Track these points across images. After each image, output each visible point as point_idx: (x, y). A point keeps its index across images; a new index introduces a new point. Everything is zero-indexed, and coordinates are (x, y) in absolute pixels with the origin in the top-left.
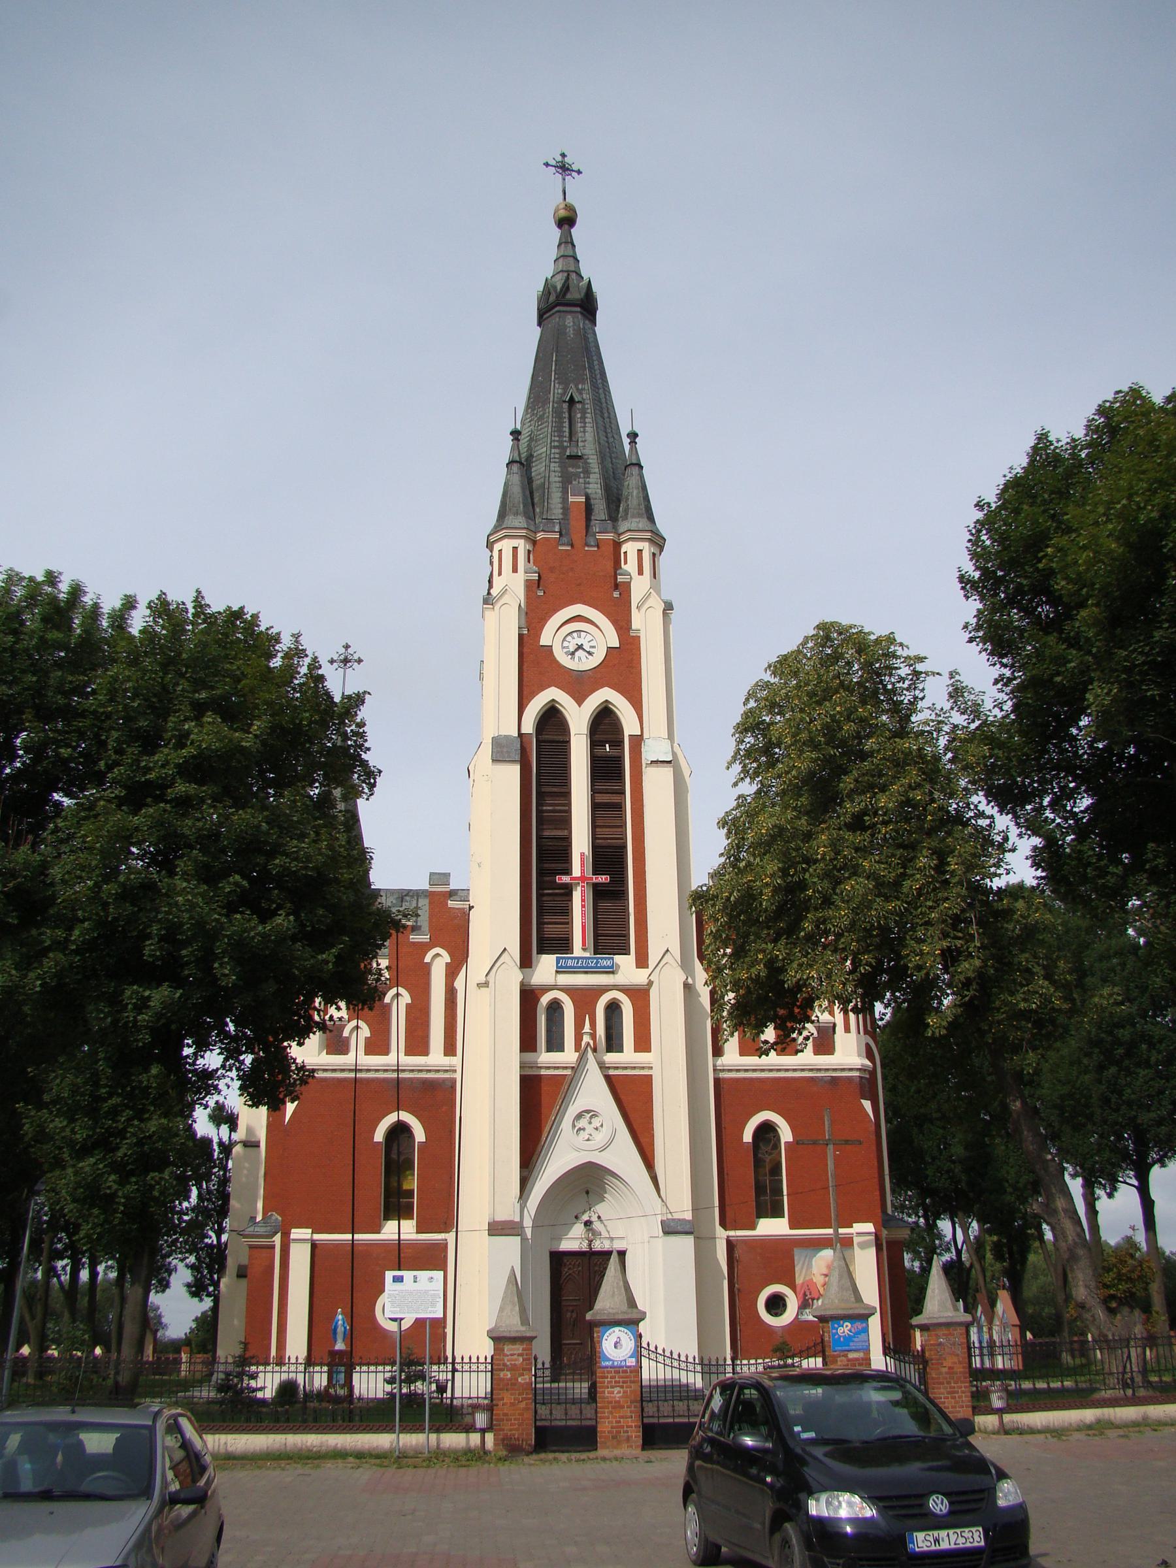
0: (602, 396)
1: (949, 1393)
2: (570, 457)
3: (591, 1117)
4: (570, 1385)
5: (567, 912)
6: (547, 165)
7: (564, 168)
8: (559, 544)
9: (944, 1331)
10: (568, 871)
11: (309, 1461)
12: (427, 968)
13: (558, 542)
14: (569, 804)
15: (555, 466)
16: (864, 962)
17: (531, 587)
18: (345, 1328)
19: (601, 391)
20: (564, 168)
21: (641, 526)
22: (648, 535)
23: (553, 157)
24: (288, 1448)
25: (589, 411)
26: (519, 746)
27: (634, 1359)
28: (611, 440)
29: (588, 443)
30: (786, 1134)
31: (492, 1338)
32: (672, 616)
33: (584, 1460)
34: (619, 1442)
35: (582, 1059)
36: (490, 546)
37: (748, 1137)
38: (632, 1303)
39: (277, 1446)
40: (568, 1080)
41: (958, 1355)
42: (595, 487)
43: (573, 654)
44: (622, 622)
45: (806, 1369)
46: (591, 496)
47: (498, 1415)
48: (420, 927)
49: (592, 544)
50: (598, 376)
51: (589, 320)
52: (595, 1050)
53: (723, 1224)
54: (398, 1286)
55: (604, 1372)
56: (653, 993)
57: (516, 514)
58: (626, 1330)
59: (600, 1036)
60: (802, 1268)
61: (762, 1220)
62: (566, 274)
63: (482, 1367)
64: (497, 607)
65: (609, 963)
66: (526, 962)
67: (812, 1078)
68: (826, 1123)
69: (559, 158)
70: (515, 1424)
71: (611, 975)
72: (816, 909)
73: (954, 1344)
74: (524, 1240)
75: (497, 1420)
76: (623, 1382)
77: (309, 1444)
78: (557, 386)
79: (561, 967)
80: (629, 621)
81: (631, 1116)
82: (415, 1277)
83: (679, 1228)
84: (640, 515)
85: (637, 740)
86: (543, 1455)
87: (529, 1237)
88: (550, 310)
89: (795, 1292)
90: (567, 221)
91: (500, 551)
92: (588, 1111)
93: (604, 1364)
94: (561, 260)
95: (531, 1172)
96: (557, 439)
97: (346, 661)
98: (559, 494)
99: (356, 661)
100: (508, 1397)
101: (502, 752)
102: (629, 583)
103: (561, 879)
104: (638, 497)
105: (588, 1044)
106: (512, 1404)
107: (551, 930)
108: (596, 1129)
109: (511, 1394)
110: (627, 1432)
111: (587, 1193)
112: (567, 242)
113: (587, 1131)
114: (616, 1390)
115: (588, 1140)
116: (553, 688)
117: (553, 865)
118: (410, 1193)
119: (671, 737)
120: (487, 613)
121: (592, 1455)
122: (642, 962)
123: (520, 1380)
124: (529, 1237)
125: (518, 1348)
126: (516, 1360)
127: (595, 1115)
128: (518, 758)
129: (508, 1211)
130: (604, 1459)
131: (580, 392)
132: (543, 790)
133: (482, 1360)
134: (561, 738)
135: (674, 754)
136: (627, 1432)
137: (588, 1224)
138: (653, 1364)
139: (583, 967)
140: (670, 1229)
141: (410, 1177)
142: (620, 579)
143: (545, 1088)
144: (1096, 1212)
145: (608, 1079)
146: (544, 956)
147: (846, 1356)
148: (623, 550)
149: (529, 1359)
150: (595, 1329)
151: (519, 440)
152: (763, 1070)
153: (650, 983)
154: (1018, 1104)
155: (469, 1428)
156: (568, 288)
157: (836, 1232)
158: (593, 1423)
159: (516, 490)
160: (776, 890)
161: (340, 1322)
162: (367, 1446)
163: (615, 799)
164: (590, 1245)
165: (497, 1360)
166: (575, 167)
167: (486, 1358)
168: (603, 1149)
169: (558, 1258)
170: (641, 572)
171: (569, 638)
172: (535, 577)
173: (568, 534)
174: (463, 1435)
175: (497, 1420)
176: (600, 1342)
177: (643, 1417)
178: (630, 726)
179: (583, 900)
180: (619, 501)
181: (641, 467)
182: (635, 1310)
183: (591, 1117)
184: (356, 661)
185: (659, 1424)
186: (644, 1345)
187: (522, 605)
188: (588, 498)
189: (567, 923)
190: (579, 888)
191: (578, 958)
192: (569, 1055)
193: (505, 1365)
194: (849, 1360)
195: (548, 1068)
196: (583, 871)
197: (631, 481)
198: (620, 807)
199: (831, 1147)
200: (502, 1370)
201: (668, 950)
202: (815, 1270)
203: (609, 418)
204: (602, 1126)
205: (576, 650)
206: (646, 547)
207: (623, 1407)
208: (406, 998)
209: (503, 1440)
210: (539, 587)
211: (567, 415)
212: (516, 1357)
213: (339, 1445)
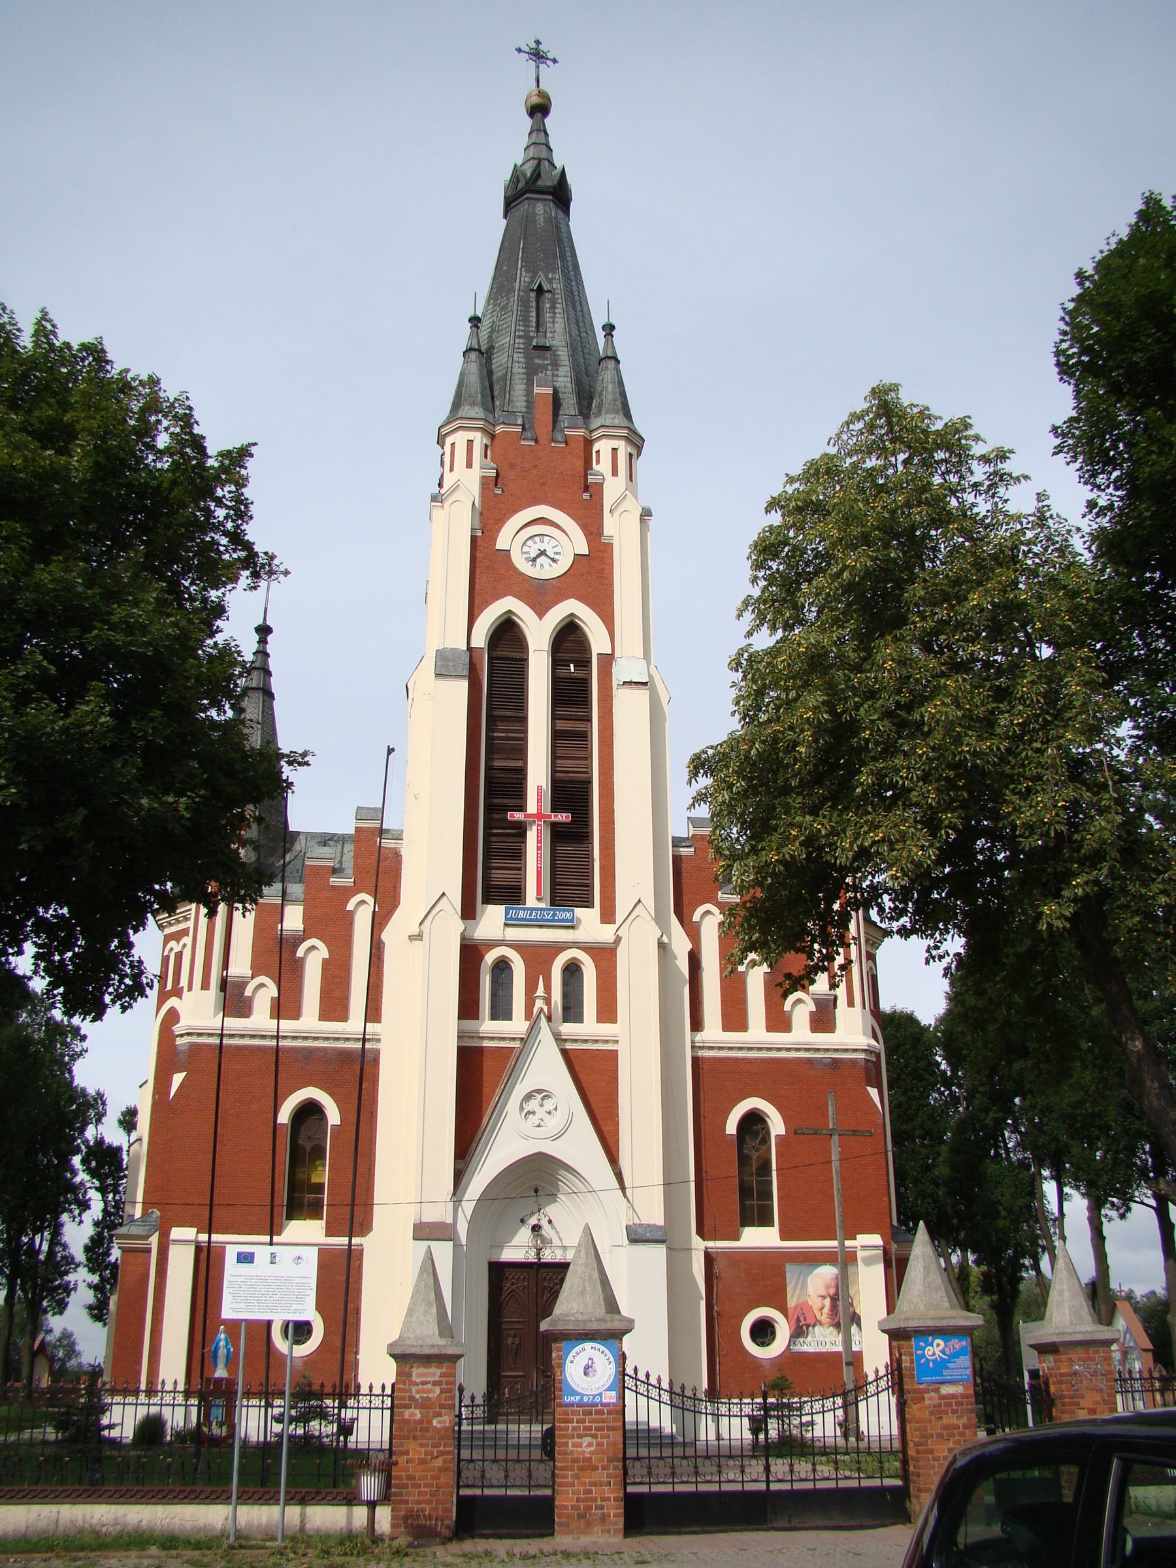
0: (575, 288)
2: (536, 348)
3: (543, 1099)
4: (513, 1427)
5: (518, 855)
6: (519, 50)
7: (538, 55)
8: (521, 439)
9: (1079, 1353)
10: (522, 808)
11: (81, 1554)
12: (350, 916)
13: (521, 437)
14: (525, 732)
16: (947, 822)
17: (487, 485)
18: (228, 1350)
19: (574, 283)
20: (538, 55)
21: (616, 422)
22: (625, 432)
23: (528, 42)
24: (61, 1529)
25: (560, 301)
26: (468, 660)
27: (614, 1393)
28: (584, 335)
29: (557, 334)
30: (777, 1126)
31: (394, 1356)
32: (650, 523)
33: (534, 1557)
34: (589, 1525)
35: (533, 1029)
36: (441, 441)
37: (731, 1128)
38: (612, 1306)
39: (43, 1524)
40: (515, 1054)
42: (564, 381)
43: (534, 560)
44: (592, 525)
46: (560, 390)
47: (400, 1478)
48: (344, 869)
49: (560, 439)
50: (571, 268)
51: (563, 211)
52: (549, 1019)
53: (701, 1232)
54: (245, 1268)
55: (566, 1413)
56: (621, 953)
57: (473, 404)
58: (602, 1348)
59: (556, 1002)
60: (795, 1287)
61: (747, 1229)
62: (536, 162)
63: (377, 1402)
64: (447, 504)
65: (568, 916)
66: (468, 912)
68: (830, 1109)
69: (534, 45)
70: (425, 1493)
71: (571, 931)
72: (875, 759)
73: (1095, 1373)
74: (458, 1246)
75: (398, 1486)
76: (597, 1429)
77: (95, 1521)
78: (524, 274)
79: (511, 919)
80: (600, 527)
81: (592, 1099)
82: (273, 1256)
83: (648, 1236)
84: (615, 412)
85: (607, 660)
86: (469, 1545)
87: (464, 1243)
88: (518, 198)
89: (786, 1316)
90: (539, 109)
91: (453, 444)
92: (539, 1091)
93: (567, 1399)
95: (467, 1164)
96: (522, 328)
98: (523, 387)
99: (282, 573)
100: (416, 1450)
101: (447, 666)
102: (602, 484)
103: (512, 816)
104: (613, 392)
105: (541, 1010)
106: (422, 1462)
107: (500, 876)
108: (549, 1113)
109: (422, 1445)
110: (602, 1507)
111: (536, 1191)
112: (539, 130)
113: (538, 1115)
114: (586, 1441)
115: (539, 1126)
116: (510, 598)
117: (505, 801)
118: (319, 1188)
119: (646, 656)
120: (435, 512)
121: (545, 1544)
122: (608, 915)
123: (435, 1422)
124: (464, 1243)
125: (434, 1372)
126: (430, 1391)
127: (546, 1095)
128: (466, 672)
129: (439, 1213)
130: (567, 1555)
131: (550, 281)
132: (494, 713)
133: (377, 1390)
134: (517, 655)
135: (650, 676)
136: (602, 1507)
137: (536, 1228)
138: (642, 1400)
140: (637, 1236)
141: (320, 1168)
142: (591, 479)
143: (487, 1063)
144: (1103, 1238)
145: (565, 1053)
146: (490, 907)
147: (937, 1390)
148: (595, 449)
149: (450, 1391)
150: (554, 1346)
151: (478, 328)
152: (750, 1049)
153: (618, 940)
154: (1138, 1044)
155: (351, 1499)
156: (539, 175)
157: (842, 1245)
158: (548, 1492)
159: (474, 379)
160: (819, 729)
161: (222, 1343)
162: (188, 1525)
163: (579, 726)
164: (538, 1254)
165: (400, 1390)
166: (550, 56)
167: (383, 1387)
168: (556, 1138)
169: (498, 1271)
170: (615, 473)
171: (530, 543)
172: (493, 473)
173: (532, 427)
174: (342, 1510)
175: (398, 1486)
176: (561, 1366)
177: (626, 1484)
178: (598, 642)
179: (539, 842)
180: (591, 399)
181: (618, 362)
182: (617, 1317)
183: (543, 1099)
184: (282, 573)
185: (651, 1495)
186: (629, 1370)
187: (477, 504)
188: (556, 392)
189: (520, 869)
190: (535, 828)
191: (532, 909)
193: (412, 1398)
194: (942, 1397)
195: (493, 1038)
196: (539, 807)
197: (606, 375)
198: (585, 736)
199: (836, 1138)
200: (408, 1407)
201: (639, 901)
202: (811, 1290)
204: (556, 1109)
205: (538, 556)
206: (621, 445)
207: (595, 1468)
208: (323, 952)
209: (406, 1518)
210: (496, 485)
211: (534, 304)
212: (429, 1386)
213: (144, 1523)
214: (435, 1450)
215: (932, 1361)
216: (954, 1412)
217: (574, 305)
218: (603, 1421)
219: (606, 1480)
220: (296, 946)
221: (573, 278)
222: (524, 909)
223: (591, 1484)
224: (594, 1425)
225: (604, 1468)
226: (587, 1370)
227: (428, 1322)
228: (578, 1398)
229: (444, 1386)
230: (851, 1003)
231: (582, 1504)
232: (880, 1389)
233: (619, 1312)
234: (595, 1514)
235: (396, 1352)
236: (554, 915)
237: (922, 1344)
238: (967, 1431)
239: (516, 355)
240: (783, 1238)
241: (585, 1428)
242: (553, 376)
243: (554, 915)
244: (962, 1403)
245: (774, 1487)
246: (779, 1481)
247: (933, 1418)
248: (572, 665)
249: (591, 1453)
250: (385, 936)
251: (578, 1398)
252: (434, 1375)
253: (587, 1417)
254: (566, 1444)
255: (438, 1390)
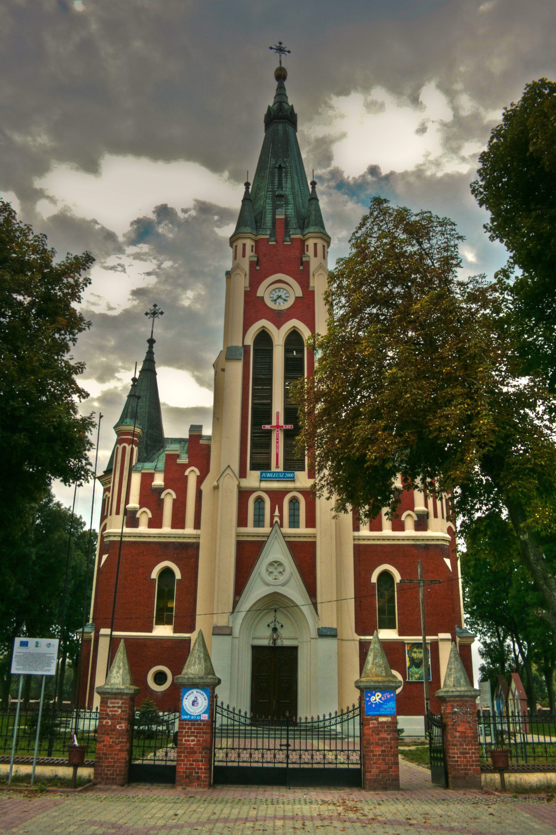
1: (461, 753)
6: (271, 48)
7: (280, 50)
10: (270, 423)
15: (269, 201)
17: (252, 265)
20: (280, 50)
22: (320, 235)
27: (206, 715)
28: (302, 188)
41: (469, 722)
43: (275, 300)
45: (127, 739)
51: (293, 127)
54: (24, 650)
58: (202, 692)
65: (292, 475)
67: (413, 545)
76: (197, 733)
79: (263, 477)
80: (308, 283)
82: (37, 643)
90: (281, 76)
92: (276, 562)
94: (277, 97)
97: (154, 314)
98: (271, 216)
103: (264, 427)
111: (275, 611)
123: (118, 727)
131: (285, 162)
134: (268, 348)
136: (198, 773)
139: (276, 478)
147: (377, 720)
148: (306, 243)
157: (424, 639)
168: (283, 585)
170: (316, 255)
172: (255, 259)
189: (268, 453)
191: (273, 473)
192: (266, 529)
193: (107, 714)
196: (278, 422)
203: (302, 176)
204: (284, 571)
205: (278, 298)
207: (196, 753)
212: (116, 709)
214: (117, 741)
215: (375, 704)
216: (385, 731)
217: (297, 173)
218: (201, 729)
219: (200, 759)
220: (160, 493)
221: (297, 160)
222: (270, 473)
223: (193, 761)
224: (196, 731)
225: (200, 753)
226: (194, 703)
227: (118, 677)
228: (188, 717)
229: (123, 709)
230: (436, 516)
231: (188, 771)
232: (355, 715)
233: (214, 674)
234: (194, 776)
235: (100, 691)
236: (285, 475)
237: (369, 695)
238: (392, 742)
239: (267, 200)
240: (400, 635)
241: (192, 732)
242: (286, 209)
243: (285, 475)
244: (390, 727)
245: (290, 766)
246: (293, 763)
247: (374, 734)
248: (295, 352)
249: (194, 745)
250: (202, 487)
251: (188, 717)
252: (118, 703)
253: (193, 727)
254: (182, 740)
255: (120, 711)
